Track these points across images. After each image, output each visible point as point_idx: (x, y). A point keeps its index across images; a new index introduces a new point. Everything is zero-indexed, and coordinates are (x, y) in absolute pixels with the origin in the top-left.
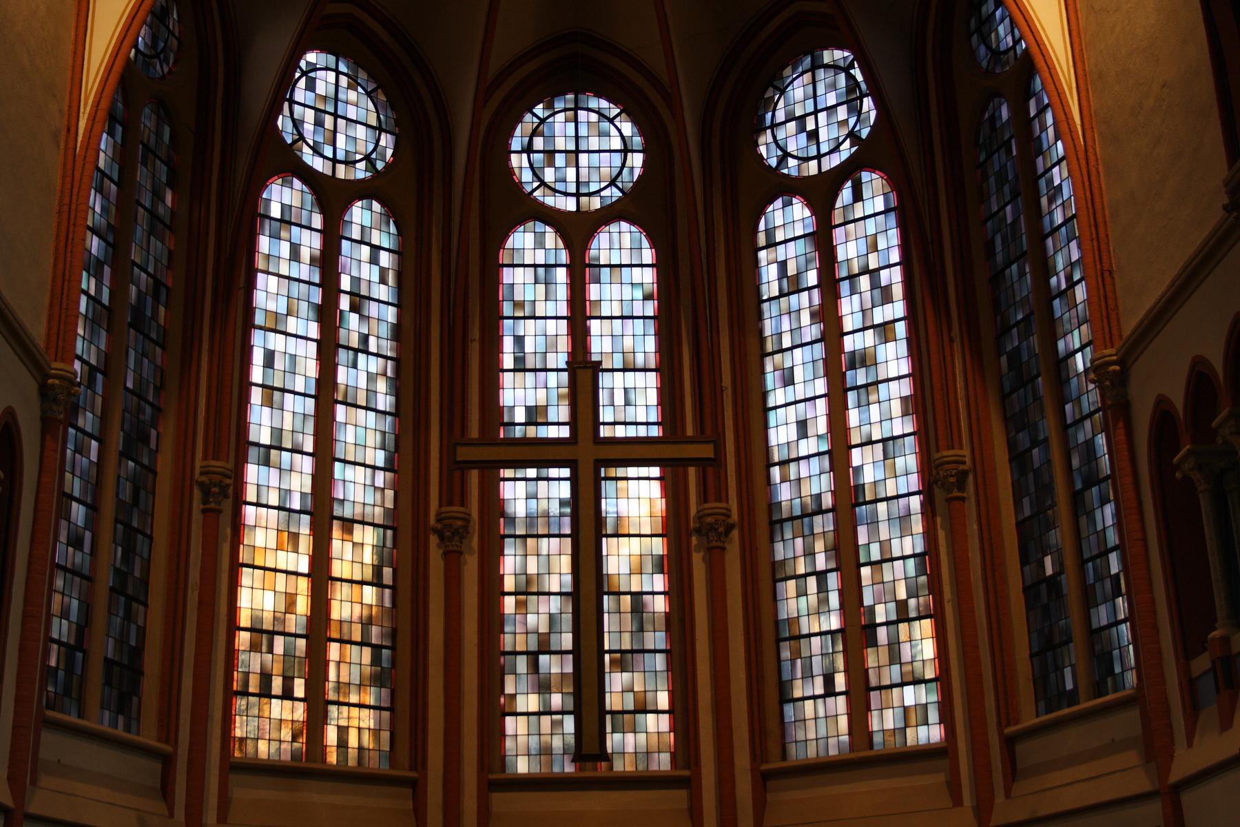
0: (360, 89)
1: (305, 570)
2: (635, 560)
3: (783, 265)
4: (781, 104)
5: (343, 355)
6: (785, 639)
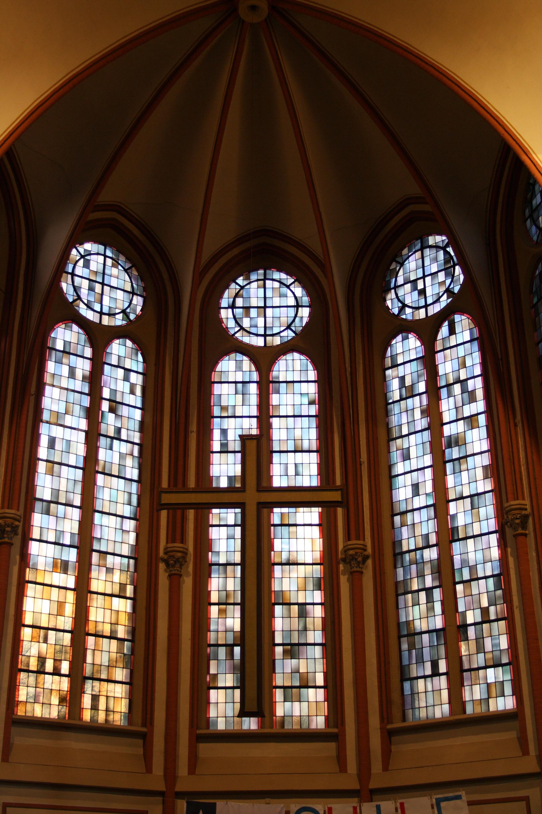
0: (120, 267)
1: (72, 586)
2: (301, 581)
3: (402, 379)
4: (401, 273)
5: (103, 441)
6: (404, 636)
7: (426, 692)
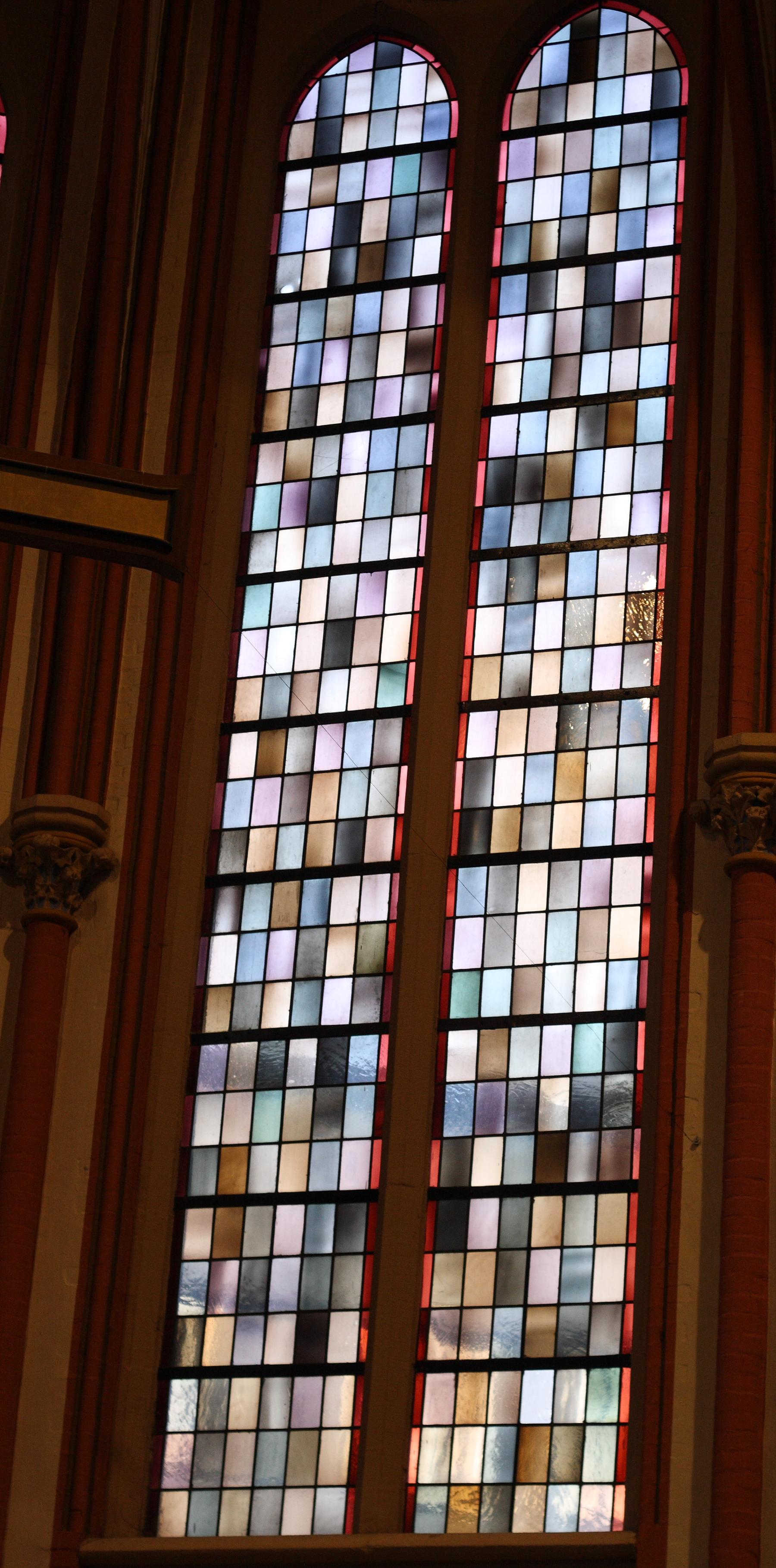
3: (349, 216)
6: (202, 1202)
7: (258, 1431)
